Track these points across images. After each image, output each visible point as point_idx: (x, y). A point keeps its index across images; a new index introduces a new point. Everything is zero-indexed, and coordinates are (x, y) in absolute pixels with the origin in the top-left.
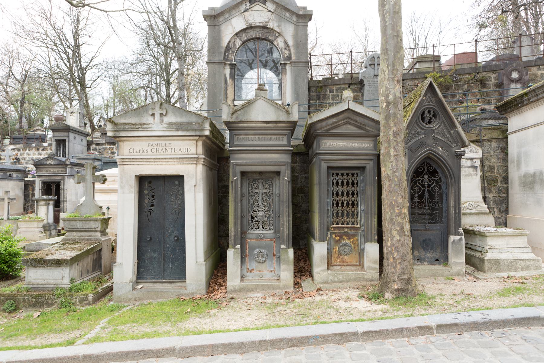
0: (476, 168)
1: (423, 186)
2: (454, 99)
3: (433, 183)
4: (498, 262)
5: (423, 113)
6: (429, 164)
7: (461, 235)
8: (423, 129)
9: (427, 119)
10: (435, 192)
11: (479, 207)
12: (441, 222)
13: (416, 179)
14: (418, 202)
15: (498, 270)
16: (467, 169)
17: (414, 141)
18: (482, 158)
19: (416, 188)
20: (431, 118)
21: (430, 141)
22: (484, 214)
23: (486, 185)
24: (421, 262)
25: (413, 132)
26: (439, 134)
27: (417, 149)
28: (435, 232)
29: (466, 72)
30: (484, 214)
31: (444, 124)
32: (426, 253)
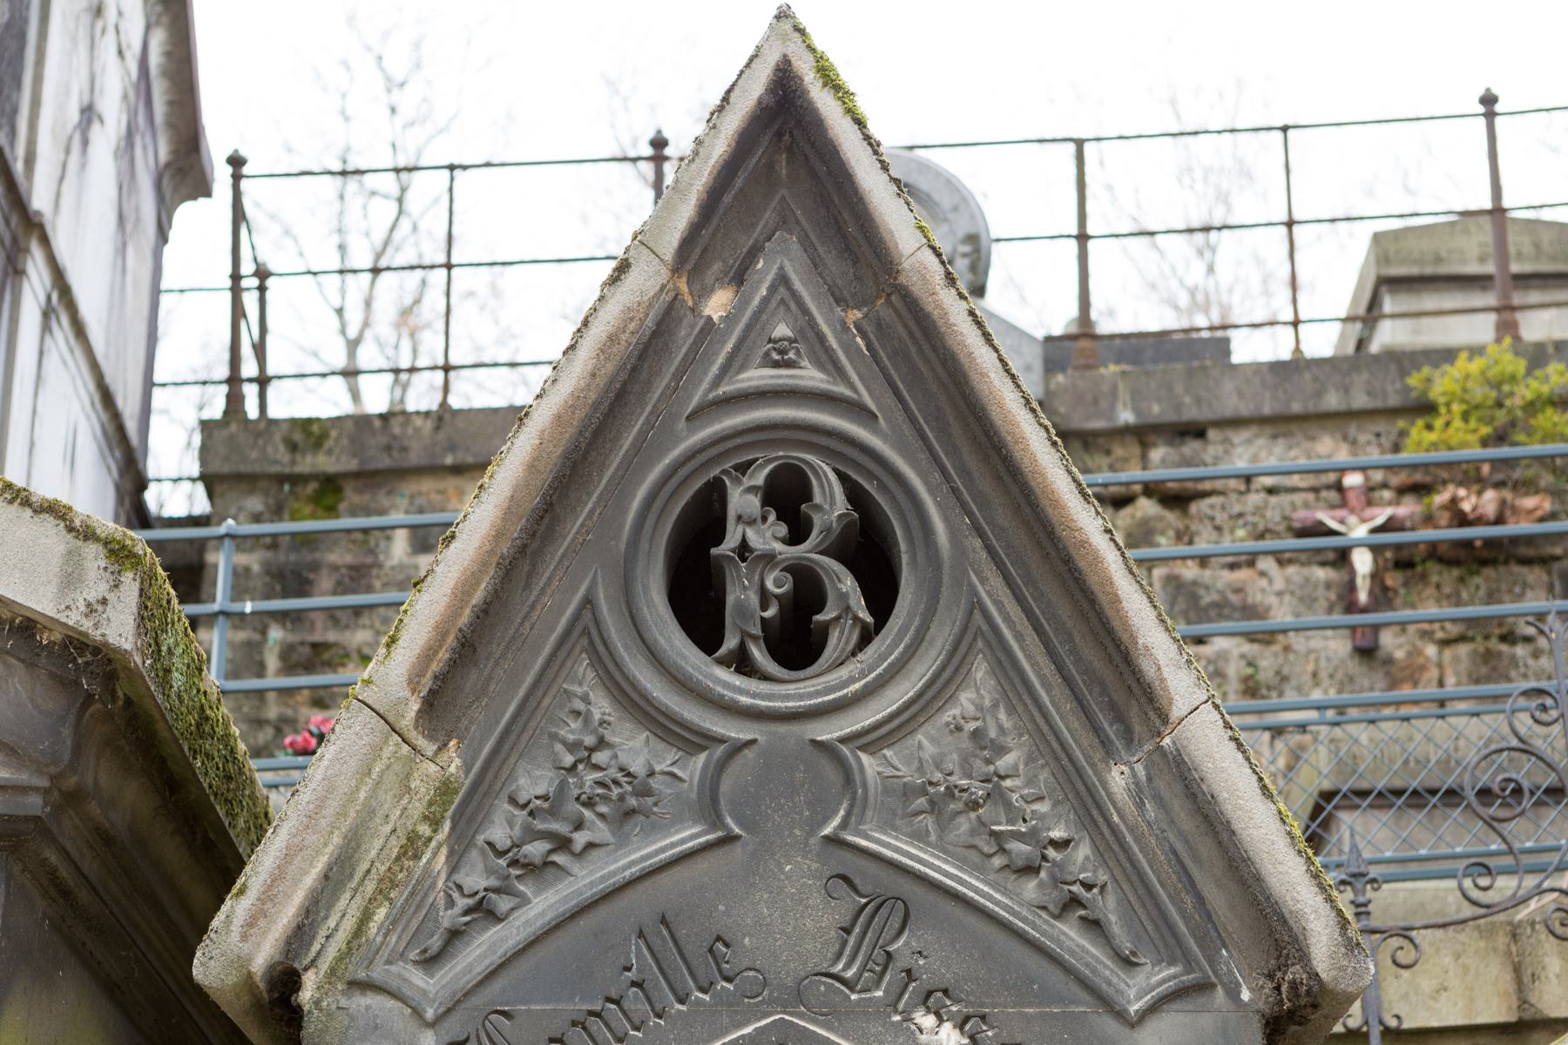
5: (703, 522)
8: (691, 740)
9: (748, 599)
17: (543, 904)
20: (807, 592)
25: (534, 781)
26: (932, 804)
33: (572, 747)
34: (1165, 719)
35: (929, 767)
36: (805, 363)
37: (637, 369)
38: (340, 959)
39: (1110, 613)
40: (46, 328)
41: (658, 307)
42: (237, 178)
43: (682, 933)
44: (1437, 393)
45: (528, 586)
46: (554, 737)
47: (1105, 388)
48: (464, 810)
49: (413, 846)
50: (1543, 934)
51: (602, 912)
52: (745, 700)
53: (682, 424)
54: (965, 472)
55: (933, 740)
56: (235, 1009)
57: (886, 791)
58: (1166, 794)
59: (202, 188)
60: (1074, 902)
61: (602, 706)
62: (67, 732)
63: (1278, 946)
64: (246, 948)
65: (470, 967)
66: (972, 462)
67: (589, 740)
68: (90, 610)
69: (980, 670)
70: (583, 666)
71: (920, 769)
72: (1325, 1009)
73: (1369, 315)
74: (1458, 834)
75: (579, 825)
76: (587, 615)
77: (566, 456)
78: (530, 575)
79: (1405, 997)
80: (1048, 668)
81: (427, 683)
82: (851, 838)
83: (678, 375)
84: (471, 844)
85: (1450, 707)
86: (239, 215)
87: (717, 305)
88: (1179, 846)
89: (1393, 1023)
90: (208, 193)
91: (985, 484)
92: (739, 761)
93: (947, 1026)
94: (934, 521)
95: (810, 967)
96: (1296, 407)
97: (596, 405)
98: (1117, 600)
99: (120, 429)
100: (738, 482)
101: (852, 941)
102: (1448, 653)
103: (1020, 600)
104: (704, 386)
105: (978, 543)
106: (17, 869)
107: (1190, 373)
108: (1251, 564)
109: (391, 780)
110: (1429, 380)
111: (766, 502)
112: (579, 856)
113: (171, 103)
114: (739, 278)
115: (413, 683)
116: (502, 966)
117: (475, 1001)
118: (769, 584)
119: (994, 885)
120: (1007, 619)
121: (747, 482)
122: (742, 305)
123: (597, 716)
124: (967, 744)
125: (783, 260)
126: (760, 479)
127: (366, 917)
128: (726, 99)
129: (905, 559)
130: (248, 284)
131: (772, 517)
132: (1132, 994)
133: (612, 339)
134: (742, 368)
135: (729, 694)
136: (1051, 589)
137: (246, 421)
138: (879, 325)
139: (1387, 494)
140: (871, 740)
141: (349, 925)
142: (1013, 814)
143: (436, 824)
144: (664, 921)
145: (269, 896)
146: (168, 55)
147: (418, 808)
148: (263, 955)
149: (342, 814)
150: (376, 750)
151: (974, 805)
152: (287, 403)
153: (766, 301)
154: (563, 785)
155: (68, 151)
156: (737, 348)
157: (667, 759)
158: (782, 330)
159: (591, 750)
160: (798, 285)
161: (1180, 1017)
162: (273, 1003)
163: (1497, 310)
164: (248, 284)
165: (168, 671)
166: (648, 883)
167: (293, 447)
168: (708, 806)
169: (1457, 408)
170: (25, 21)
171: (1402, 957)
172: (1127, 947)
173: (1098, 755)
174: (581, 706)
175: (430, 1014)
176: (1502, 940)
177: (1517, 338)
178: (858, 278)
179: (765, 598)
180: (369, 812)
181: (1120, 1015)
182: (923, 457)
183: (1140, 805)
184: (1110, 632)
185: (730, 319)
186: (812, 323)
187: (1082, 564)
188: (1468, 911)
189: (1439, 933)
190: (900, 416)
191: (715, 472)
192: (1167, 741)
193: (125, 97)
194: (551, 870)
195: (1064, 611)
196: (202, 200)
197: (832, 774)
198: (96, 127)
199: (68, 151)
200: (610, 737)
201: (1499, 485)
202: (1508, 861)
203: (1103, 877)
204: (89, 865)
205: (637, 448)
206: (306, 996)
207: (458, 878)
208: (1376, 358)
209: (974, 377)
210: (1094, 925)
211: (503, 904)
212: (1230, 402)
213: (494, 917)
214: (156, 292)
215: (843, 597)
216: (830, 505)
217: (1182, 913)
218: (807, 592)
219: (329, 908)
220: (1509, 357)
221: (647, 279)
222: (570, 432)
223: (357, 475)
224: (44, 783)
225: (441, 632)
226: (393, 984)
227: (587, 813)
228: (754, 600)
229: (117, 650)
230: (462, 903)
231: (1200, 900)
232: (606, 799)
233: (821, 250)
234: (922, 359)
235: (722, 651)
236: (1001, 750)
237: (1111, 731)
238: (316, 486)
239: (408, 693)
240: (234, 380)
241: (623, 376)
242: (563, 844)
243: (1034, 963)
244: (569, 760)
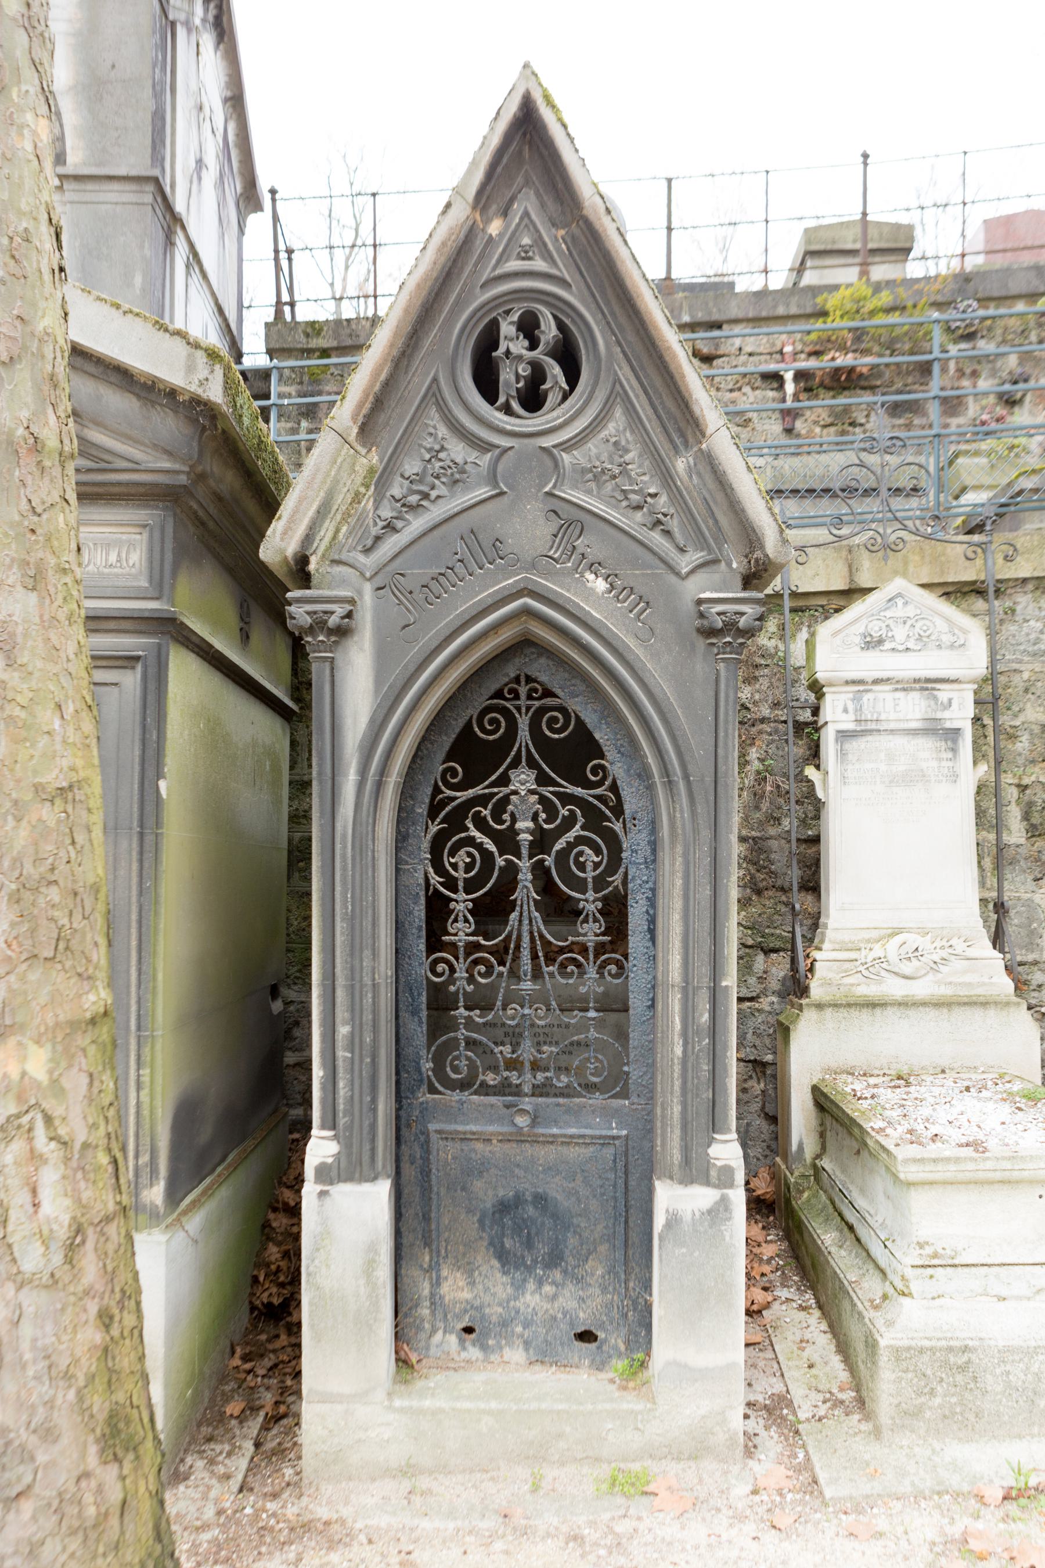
0: (953, 735)
1: (507, 841)
2: (954, 422)
3: (569, 823)
4: (963, 1369)
5: (489, 339)
6: (548, 693)
7: (725, 1178)
8: (484, 447)
9: (510, 378)
10: (580, 885)
11: (958, 965)
12: (616, 1083)
13: (463, 796)
14: (472, 948)
15: (965, 1420)
16: (900, 741)
17: (417, 524)
18: (992, 677)
19: (462, 857)
20: (538, 374)
21: (529, 529)
22: (984, 1004)
23: (1016, 834)
24: (484, 1348)
25: (412, 467)
26: (596, 476)
27: (433, 587)
28: (573, 1153)
29: (1014, 288)
30: (984, 1004)
31: (631, 411)
32: (519, 1287)
33: (429, 450)
34: (703, 435)
35: (594, 459)
36: (537, 257)
37: (455, 263)
38: (326, 550)
39: (680, 383)
40: (188, 273)
41: (466, 229)
42: (274, 200)
43: (480, 537)
44: (829, 306)
45: (406, 372)
46: (420, 445)
47: (677, 304)
48: (381, 479)
49: (357, 498)
50: (863, 550)
51: (444, 527)
52: (509, 427)
53: (478, 289)
54: (613, 314)
55: (596, 446)
56: (280, 573)
57: (574, 470)
58: (702, 471)
59: (258, 207)
60: (659, 522)
61: (442, 431)
62: (195, 444)
63: (751, 542)
64: (283, 545)
65: (385, 554)
66: (617, 309)
67: (437, 447)
68: (201, 384)
69: (618, 412)
70: (433, 411)
71: (590, 460)
72: (770, 572)
73: (800, 270)
74: (827, 507)
75: (433, 488)
76: (435, 386)
77: (423, 305)
78: (408, 366)
79: (800, 578)
80: (648, 408)
81: (360, 420)
82: (557, 493)
83: (476, 265)
84: (384, 496)
85: (825, 447)
86: (276, 218)
87: (495, 227)
88: (707, 496)
89: (794, 589)
90: (262, 210)
91: (623, 319)
92: (506, 456)
93: (600, 579)
94: (599, 341)
95: (539, 553)
96: (764, 314)
97: (436, 279)
98: (683, 376)
99: (228, 326)
100: (505, 319)
101: (557, 540)
102: (825, 431)
103: (638, 378)
104: (489, 270)
105: (619, 349)
106: (178, 511)
107: (716, 297)
108: (740, 389)
109: (346, 466)
110: (826, 300)
111: (519, 329)
112: (433, 502)
113: (240, 162)
114: (505, 213)
115: (354, 420)
116: (400, 552)
117: (388, 569)
118: (520, 371)
119: (622, 515)
120: (631, 387)
121: (509, 319)
122: (506, 227)
123: (440, 435)
124: (611, 448)
125: (527, 203)
126: (515, 317)
127: (337, 531)
128: (498, 113)
129: (584, 358)
130: (283, 257)
131: (521, 337)
132: (683, 564)
133: (444, 244)
134: (507, 261)
135: (501, 425)
136: (651, 371)
137: (285, 322)
138: (574, 238)
139: (803, 356)
140: (567, 446)
141: (330, 534)
142: (632, 481)
143: (367, 487)
144: (472, 531)
145: (292, 520)
146: (237, 135)
147: (359, 480)
148: (291, 548)
149: (324, 482)
150: (339, 451)
151: (614, 477)
152: (305, 313)
153: (518, 225)
154: (425, 469)
155: (191, 182)
156: (504, 250)
157: (473, 456)
158: (526, 241)
159: (438, 452)
160: (534, 217)
161: (705, 575)
162: (298, 571)
163: (861, 265)
164: (283, 257)
165: (241, 416)
166: (465, 514)
167: (307, 335)
168: (492, 478)
169: (838, 313)
170: (165, 111)
171: (800, 560)
172: (682, 543)
173: (672, 453)
174: (432, 431)
175: (368, 575)
176: (844, 553)
177: (868, 280)
178: (563, 213)
179: (518, 378)
180: (336, 481)
181: (678, 574)
182: (593, 306)
183: (691, 477)
184: (679, 392)
185: (501, 235)
186: (541, 237)
187: (667, 359)
188: (832, 538)
189: (817, 550)
190: (582, 285)
191: (494, 314)
192: (704, 446)
193: (218, 156)
194: (421, 509)
195: (658, 382)
196: (259, 213)
197: (549, 462)
198: (204, 170)
199: (191, 182)
200: (446, 446)
201: (855, 351)
202: (850, 518)
203: (672, 511)
204: (212, 510)
205: (457, 302)
206: (312, 567)
207: (379, 512)
208: (803, 289)
209: (619, 263)
210: (667, 533)
211: (399, 524)
212: (734, 312)
213: (395, 530)
214: (240, 260)
215: (555, 376)
216: (549, 331)
217: (708, 527)
218: (538, 374)
219: (321, 526)
220: (864, 287)
221: (461, 212)
222: (424, 293)
223: (337, 349)
224: (187, 469)
225: (366, 395)
226: (351, 561)
227: (437, 482)
228: (513, 378)
229: (215, 404)
230: (381, 524)
231: (716, 521)
232: (445, 475)
233: (545, 198)
234: (594, 254)
235: (498, 404)
236: (627, 451)
237: (678, 441)
238: (315, 350)
239: (351, 424)
240: (279, 304)
241: (449, 264)
242: (426, 496)
243: (640, 550)
244: (427, 456)
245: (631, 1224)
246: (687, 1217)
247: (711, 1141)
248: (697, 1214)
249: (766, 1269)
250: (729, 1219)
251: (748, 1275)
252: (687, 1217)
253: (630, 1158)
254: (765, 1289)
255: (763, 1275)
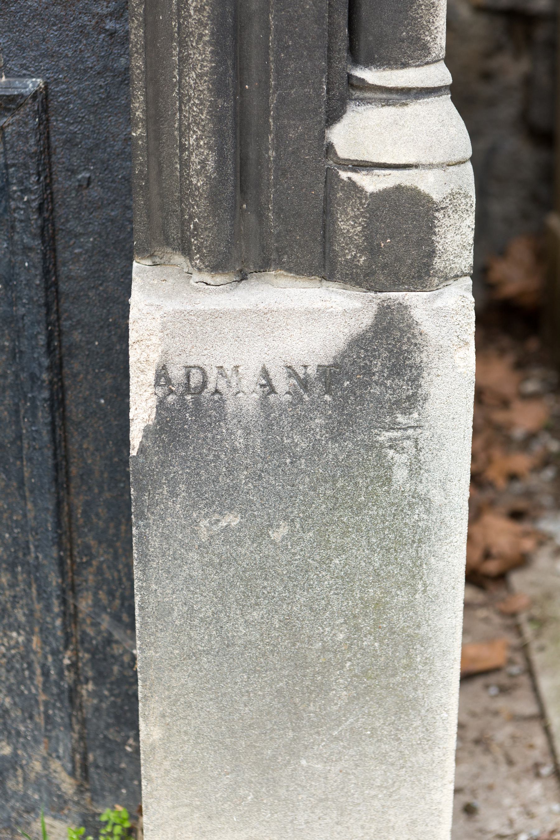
245: (75, 412)
246: (245, 398)
247: (343, 95)
248: (282, 384)
249: (520, 462)
250: (412, 402)
251: (477, 480)
252: (245, 398)
253: (62, 183)
254: (516, 515)
255: (513, 477)
